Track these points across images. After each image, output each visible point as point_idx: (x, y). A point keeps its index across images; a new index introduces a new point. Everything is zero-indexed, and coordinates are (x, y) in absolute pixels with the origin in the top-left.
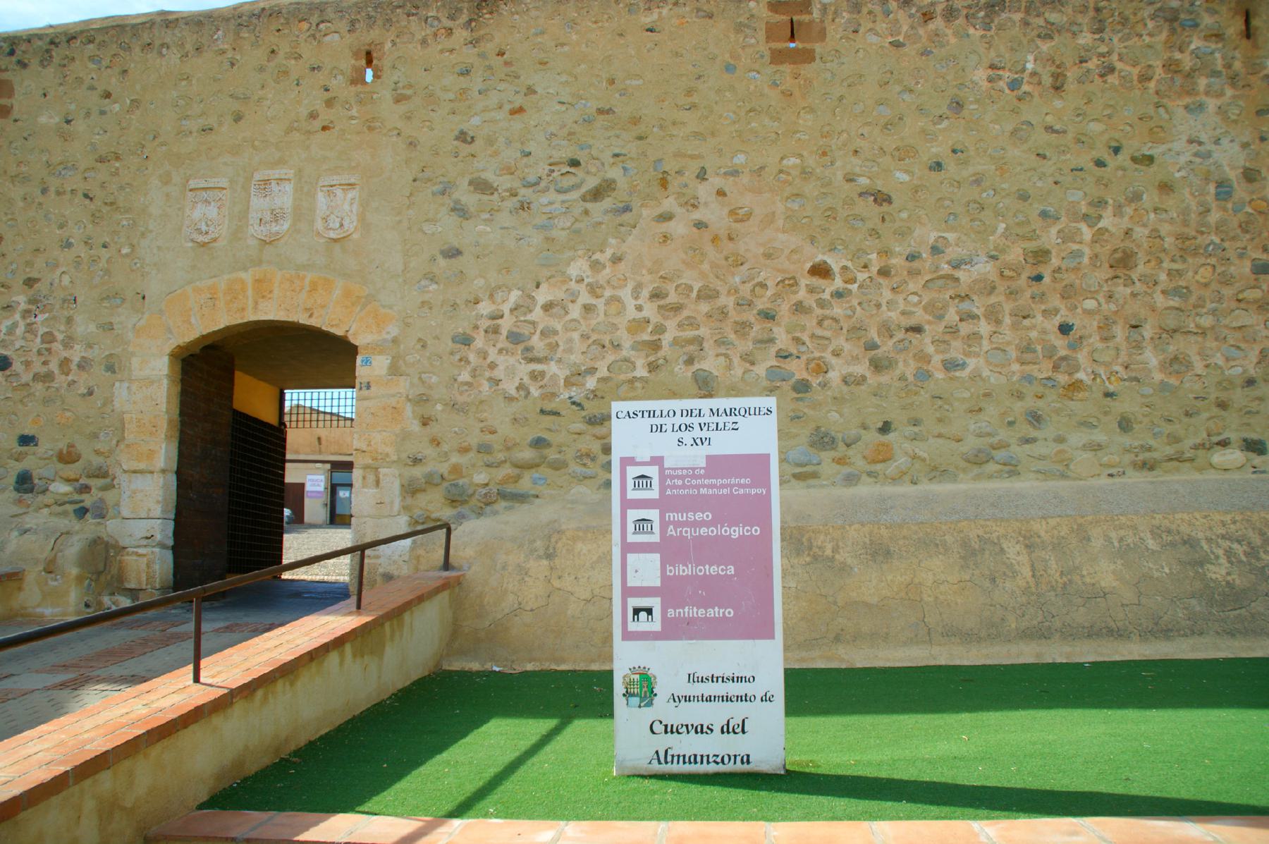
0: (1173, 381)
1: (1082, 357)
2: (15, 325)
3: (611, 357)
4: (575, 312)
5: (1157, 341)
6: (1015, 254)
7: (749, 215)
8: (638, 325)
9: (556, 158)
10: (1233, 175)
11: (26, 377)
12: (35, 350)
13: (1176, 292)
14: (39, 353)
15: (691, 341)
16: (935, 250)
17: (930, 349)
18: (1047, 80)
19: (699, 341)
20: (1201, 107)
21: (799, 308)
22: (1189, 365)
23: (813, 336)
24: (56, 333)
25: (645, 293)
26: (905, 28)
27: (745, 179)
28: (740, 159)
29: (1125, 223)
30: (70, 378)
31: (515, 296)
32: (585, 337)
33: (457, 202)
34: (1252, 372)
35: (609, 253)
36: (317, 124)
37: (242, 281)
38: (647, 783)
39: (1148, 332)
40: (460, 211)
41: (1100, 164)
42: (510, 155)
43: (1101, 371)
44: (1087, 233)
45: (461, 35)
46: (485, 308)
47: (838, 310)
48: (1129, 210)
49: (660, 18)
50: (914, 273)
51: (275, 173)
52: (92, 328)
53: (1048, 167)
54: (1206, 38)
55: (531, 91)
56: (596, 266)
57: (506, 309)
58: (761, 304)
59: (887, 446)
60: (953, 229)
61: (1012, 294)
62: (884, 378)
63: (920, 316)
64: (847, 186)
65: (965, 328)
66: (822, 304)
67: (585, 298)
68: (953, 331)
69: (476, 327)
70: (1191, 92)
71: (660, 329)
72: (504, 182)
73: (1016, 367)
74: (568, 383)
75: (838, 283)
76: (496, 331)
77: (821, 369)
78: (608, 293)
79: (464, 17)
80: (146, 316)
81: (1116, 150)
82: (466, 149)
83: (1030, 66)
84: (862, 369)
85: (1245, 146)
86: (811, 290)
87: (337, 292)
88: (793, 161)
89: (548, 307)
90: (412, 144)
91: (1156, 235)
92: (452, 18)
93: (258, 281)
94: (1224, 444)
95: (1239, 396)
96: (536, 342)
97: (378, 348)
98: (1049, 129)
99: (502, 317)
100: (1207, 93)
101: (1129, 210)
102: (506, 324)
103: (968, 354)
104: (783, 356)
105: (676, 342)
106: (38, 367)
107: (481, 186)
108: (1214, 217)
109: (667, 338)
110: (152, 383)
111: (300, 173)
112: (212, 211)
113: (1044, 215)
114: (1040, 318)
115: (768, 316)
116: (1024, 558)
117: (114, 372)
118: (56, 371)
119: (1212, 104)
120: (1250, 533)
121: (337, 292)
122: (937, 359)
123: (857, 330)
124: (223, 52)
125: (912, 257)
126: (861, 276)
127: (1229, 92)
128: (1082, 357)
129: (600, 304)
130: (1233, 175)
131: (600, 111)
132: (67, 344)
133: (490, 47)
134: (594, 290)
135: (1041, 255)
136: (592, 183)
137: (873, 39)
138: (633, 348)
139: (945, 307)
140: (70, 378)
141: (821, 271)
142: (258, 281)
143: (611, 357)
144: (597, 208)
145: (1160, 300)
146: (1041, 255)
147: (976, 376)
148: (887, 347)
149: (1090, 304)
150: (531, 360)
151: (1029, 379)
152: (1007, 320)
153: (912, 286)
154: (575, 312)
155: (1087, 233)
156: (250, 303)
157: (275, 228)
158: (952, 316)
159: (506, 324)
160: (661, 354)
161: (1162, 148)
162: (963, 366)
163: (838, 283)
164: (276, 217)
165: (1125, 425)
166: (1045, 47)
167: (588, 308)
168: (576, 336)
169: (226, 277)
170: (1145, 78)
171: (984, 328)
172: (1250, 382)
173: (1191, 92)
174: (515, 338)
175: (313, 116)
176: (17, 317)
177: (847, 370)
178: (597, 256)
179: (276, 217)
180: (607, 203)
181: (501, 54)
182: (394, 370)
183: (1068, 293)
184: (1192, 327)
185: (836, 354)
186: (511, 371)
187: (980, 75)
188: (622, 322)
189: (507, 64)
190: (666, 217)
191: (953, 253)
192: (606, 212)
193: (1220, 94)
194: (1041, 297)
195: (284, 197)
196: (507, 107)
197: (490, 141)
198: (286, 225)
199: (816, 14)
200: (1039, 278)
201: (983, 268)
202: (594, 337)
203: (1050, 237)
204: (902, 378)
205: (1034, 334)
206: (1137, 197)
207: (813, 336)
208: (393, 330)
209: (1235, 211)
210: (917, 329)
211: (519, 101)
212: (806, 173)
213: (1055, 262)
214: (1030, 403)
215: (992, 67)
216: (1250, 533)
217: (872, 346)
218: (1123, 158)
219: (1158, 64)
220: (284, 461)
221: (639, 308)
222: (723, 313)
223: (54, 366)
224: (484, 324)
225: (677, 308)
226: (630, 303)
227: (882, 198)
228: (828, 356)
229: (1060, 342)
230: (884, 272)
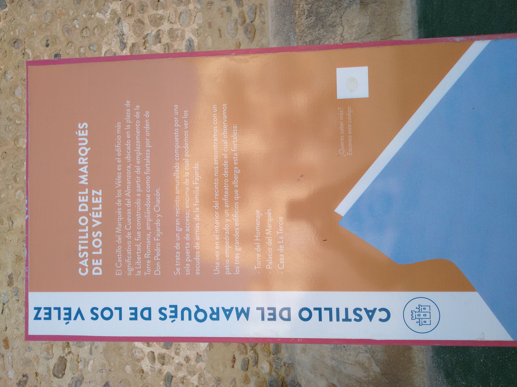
46: (146, 365)
65: (165, 39)
76: (162, 357)
103: (183, 37)
152: (160, 12)
171: (165, 27)
197: (27, 362)
201: (126, 27)
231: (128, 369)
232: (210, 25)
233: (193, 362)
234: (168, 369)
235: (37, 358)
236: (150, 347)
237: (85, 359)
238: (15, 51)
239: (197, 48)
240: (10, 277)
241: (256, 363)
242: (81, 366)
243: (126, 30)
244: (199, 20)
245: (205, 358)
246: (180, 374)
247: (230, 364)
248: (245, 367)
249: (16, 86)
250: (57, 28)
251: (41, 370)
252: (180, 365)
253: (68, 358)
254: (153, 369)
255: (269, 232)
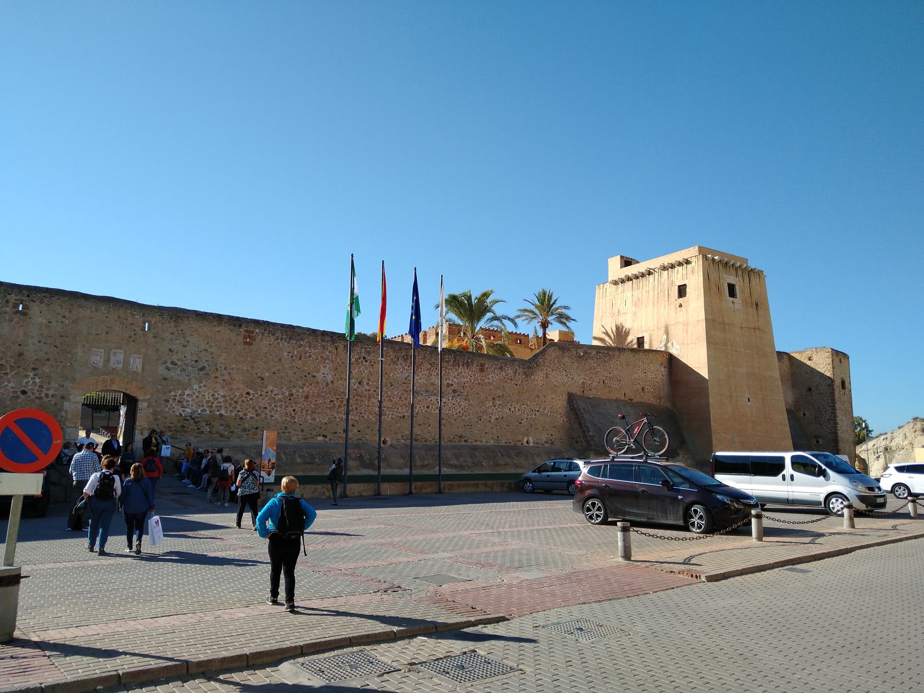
0: (312, 422)
1: (296, 416)
2: (29, 381)
3: (202, 408)
4: (194, 397)
5: (311, 415)
6: (287, 394)
7: (234, 379)
8: (208, 402)
9: (193, 359)
10: (329, 381)
11: (33, 397)
12: (36, 390)
13: (315, 405)
14: (37, 391)
15: (219, 406)
16: (271, 391)
17: (268, 412)
18: (298, 357)
19: (221, 406)
20: (326, 366)
21: (243, 401)
22: (316, 419)
23: (245, 408)
24: (44, 386)
25: (210, 395)
26: (272, 341)
27: (234, 371)
28: (234, 366)
29: (308, 389)
30: (49, 399)
31: (180, 391)
32: (196, 403)
33: (168, 366)
34: (326, 422)
35: (203, 384)
36: (131, 339)
37: (107, 379)
38: (224, 524)
39: (309, 412)
40: (168, 369)
41: (306, 376)
42: (180, 356)
43: (300, 420)
44: (301, 391)
45: (173, 324)
46: (173, 393)
47: (250, 403)
48: (309, 387)
49: (221, 329)
50: (267, 396)
51: (119, 351)
52: (57, 386)
53: (296, 376)
54: (329, 352)
55: (188, 342)
56: (200, 387)
57: (178, 394)
58: (235, 400)
59: (257, 432)
60: (275, 387)
61: (285, 402)
62: (258, 418)
63: (267, 405)
64: (256, 375)
65: (275, 408)
66: (247, 401)
67: (197, 394)
68: (273, 409)
69: (170, 398)
70: (325, 363)
71: (213, 403)
72: (179, 363)
73: (284, 417)
74: (319, 391)
75: (251, 396)
76: (175, 399)
77: (246, 415)
78: (202, 394)
79: (174, 319)
80: (75, 385)
81: (309, 374)
82: (171, 353)
83: (295, 353)
84: (254, 415)
85: (332, 376)
86: (245, 397)
87: (134, 385)
88: (245, 368)
89: (187, 395)
90: (157, 350)
91: (314, 392)
92: (170, 319)
93: (111, 379)
94: (320, 435)
95: (324, 426)
96: (184, 403)
97: (144, 401)
98: (297, 367)
99: (177, 396)
100: (327, 364)
101: (309, 387)
102: (178, 398)
103: (275, 414)
104: (238, 411)
105: (216, 406)
106: (37, 395)
107: (173, 363)
108: (325, 389)
109: (214, 405)
110: (77, 403)
111: (125, 351)
112: (98, 358)
113: (293, 386)
114: (290, 408)
115: (236, 402)
116: (284, 457)
117: (64, 399)
118: (44, 397)
119: (328, 366)
120: (323, 453)
121: (134, 385)
122: (269, 415)
123: (254, 408)
124: (104, 313)
125: (266, 392)
126: (256, 396)
127: (331, 364)
128: (296, 416)
129: (200, 396)
130: (329, 381)
131: (204, 350)
132: (48, 389)
133: (180, 329)
134: (199, 392)
135: (292, 395)
136: (200, 367)
137: (266, 342)
138: (207, 407)
139: (272, 404)
140: (49, 399)
141: (248, 393)
142: (111, 379)
143: (202, 408)
144: (201, 373)
145: (312, 406)
146: (292, 395)
147: (276, 419)
148: (259, 411)
149: (299, 406)
150: (182, 407)
151: (286, 420)
152: (283, 408)
153: (266, 399)
154: (194, 397)
155: (301, 391)
156: (109, 384)
157: (118, 366)
158: (273, 405)
159: (178, 398)
160: (213, 409)
161: (317, 374)
162: (274, 416)
163: (251, 396)
164: (118, 363)
165: (302, 431)
166: (299, 349)
167: (197, 397)
168: (194, 403)
169: (101, 377)
170: (317, 359)
171: (279, 409)
172: (326, 424)
173: (325, 363)
174: (179, 402)
175: (130, 337)
176: (30, 379)
177: (251, 416)
178: (200, 385)
179: (118, 363)
180: (203, 372)
181: (182, 331)
182: (148, 406)
183: (296, 403)
184: (317, 412)
185: (249, 412)
186: (178, 409)
187: (286, 354)
188: (205, 401)
189: (183, 334)
190: (216, 377)
191: (274, 392)
192: (203, 374)
193: (329, 364)
194: (290, 403)
195: (121, 357)
196: (182, 344)
197: (177, 353)
198: (121, 366)
199: (254, 334)
200: (290, 399)
201: (280, 396)
202: (198, 403)
203: (294, 391)
204: (262, 418)
205: (288, 411)
206: (311, 384)
207: (245, 408)
208: (149, 397)
209: (329, 389)
210: (266, 408)
211: (185, 343)
212: (248, 371)
213: (294, 396)
214: (285, 425)
215: (288, 352)
216: (323, 453)
217: (257, 411)
218: (310, 376)
219: (319, 356)
220: (16, 621)
221: (209, 398)
222: (227, 401)
223: (43, 395)
224: (172, 398)
225: (217, 399)
226: (207, 397)
227: (262, 379)
228: (247, 412)
229: (293, 413)
230: (261, 395)
231: (172, 387)
232: (278, 423)
233: (172, 410)
234: (171, 400)
235: (178, 356)
236: (212, 494)
237: (170, 349)
238: (278, 359)
239: (239, 428)
240: (206, 350)
241: (170, 431)
242: (174, 371)
243: (279, 396)
244: (280, 420)
245: (174, 414)
246: (169, 405)
247: (171, 422)
248: (169, 427)
249: (267, 359)
250: (283, 374)
251: (174, 357)
252: (172, 405)
253: (177, 367)
254: (171, 396)
255: (693, 267)
